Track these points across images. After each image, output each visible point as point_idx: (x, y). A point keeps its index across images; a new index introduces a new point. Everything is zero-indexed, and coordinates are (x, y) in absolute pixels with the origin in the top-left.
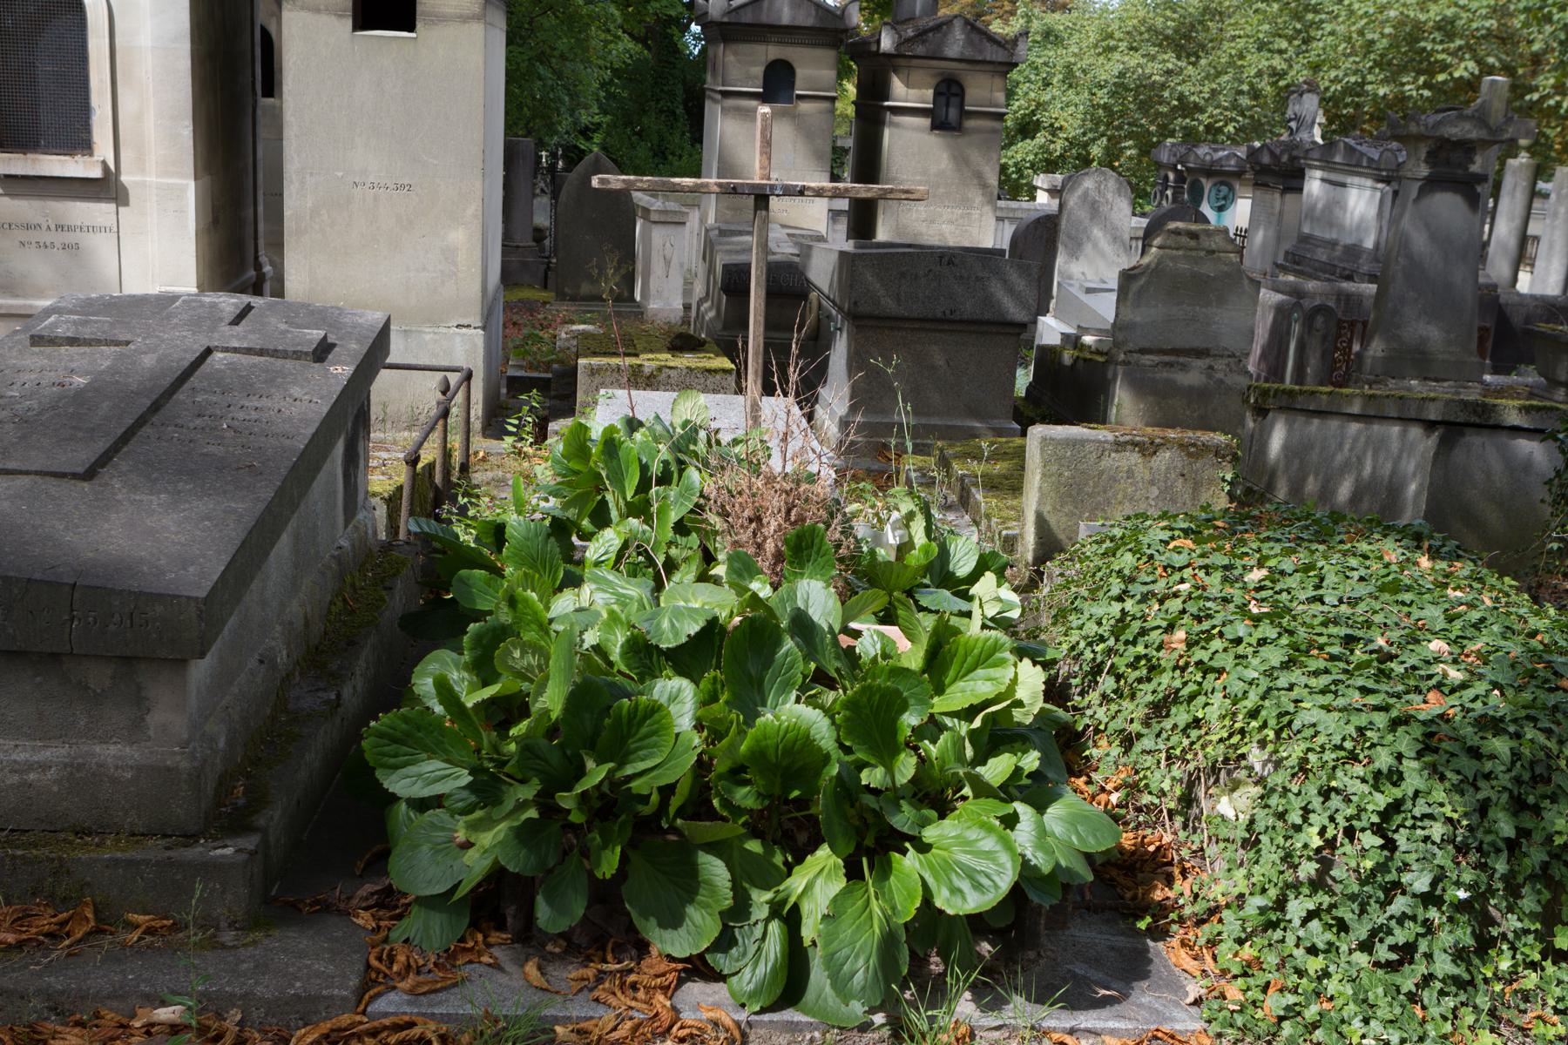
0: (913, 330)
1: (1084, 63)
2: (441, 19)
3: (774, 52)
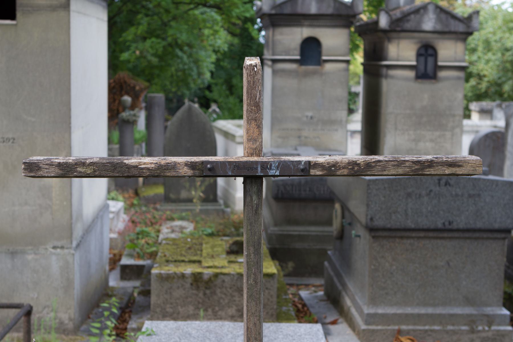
0: (419, 238)
1: (497, 37)
2: (37, 9)
3: (306, 32)
